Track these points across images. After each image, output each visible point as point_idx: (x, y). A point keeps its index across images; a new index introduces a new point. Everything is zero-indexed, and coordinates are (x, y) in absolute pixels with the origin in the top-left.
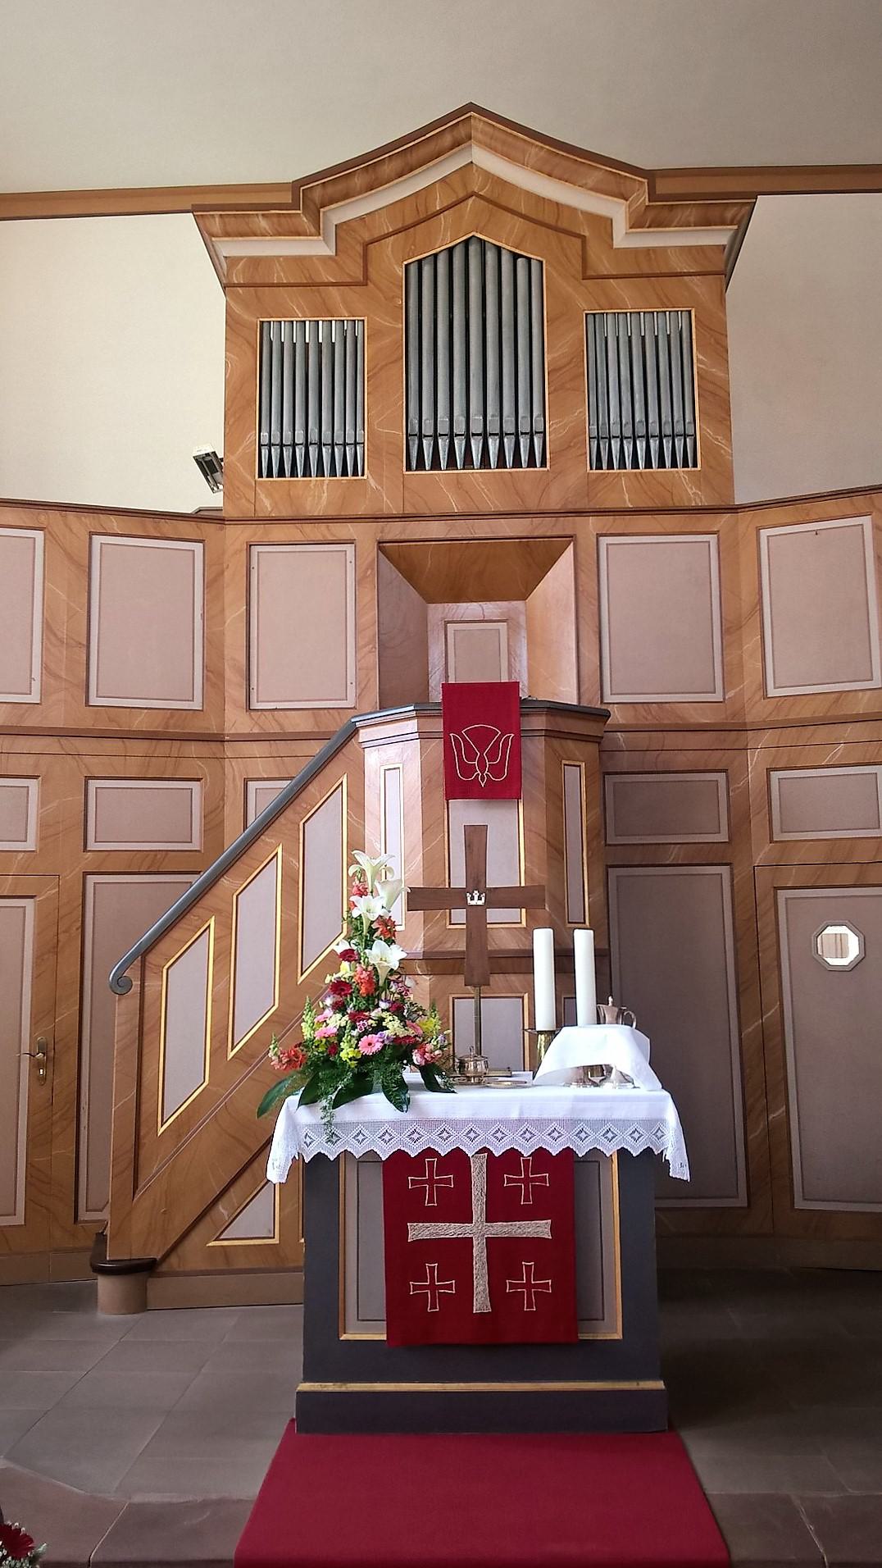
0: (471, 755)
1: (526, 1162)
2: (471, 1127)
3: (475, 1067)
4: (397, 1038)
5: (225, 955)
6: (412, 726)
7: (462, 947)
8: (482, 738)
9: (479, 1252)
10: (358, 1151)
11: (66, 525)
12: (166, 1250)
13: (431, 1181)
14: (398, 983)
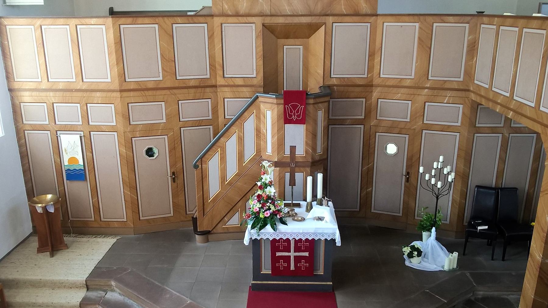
0: (291, 112)
5: (223, 159)
8: (294, 107)
11: (165, 22)
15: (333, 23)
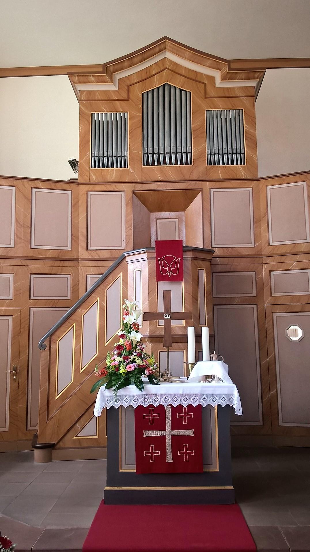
0: (165, 266)
1: (185, 409)
2: (166, 397)
3: (167, 376)
4: (140, 365)
5: (79, 336)
6: (145, 256)
7: (162, 333)
8: (169, 260)
9: (168, 441)
10: (126, 405)
11: (23, 185)
12: (58, 440)
13: (151, 416)
14: (140, 346)
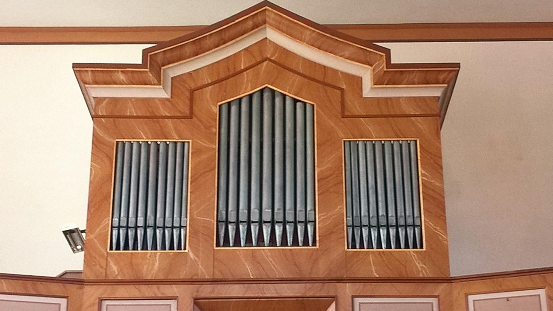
15: (353, 297)
